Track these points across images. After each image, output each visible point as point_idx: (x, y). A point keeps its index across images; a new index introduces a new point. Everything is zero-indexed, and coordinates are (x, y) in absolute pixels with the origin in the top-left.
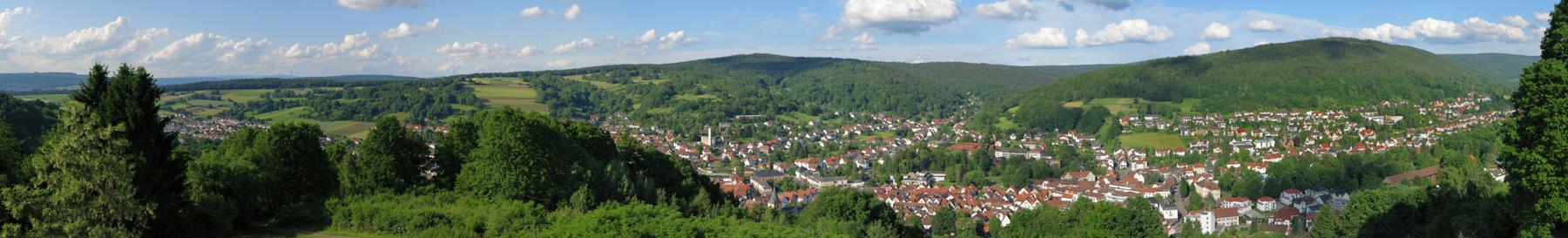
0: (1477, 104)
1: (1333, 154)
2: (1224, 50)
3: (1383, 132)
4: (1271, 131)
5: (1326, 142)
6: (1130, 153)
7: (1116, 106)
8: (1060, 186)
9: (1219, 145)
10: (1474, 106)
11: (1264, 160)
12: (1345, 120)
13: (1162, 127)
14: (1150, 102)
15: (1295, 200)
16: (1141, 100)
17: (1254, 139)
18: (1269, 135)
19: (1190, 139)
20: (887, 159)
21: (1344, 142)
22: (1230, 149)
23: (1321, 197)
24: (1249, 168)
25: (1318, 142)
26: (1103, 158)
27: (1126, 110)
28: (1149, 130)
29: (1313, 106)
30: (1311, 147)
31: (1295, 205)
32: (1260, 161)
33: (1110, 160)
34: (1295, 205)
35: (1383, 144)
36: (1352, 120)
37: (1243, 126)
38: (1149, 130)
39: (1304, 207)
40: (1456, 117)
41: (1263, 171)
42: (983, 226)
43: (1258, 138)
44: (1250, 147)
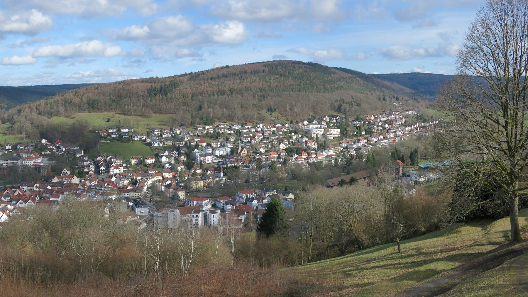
8: (49, 187)
21: (289, 151)
26: (85, 164)
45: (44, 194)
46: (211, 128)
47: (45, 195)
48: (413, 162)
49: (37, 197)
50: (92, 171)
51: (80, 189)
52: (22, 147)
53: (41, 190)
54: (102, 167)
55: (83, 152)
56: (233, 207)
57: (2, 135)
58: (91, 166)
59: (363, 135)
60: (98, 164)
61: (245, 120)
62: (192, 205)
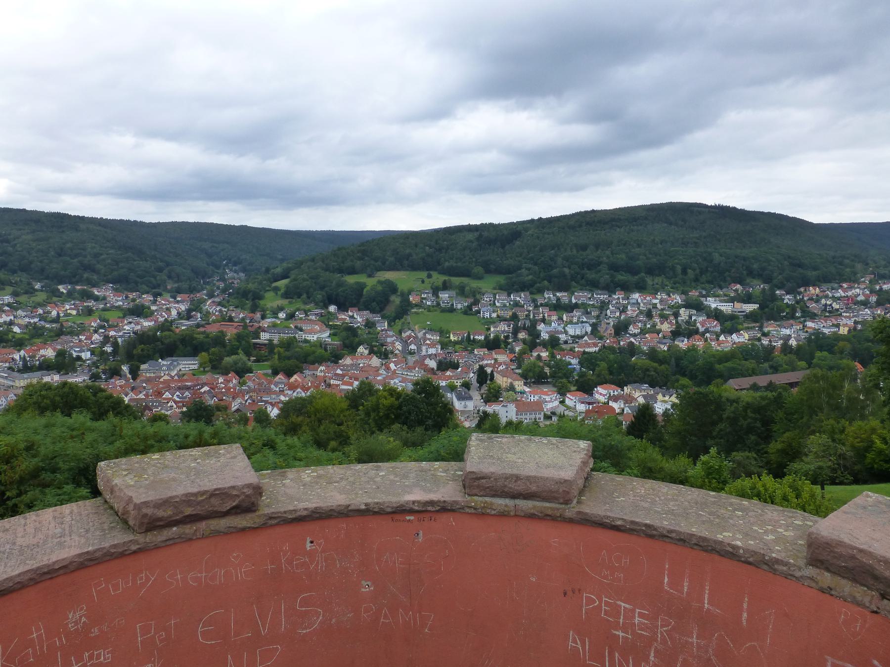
0: (872, 291)
1: (662, 346)
2: (536, 218)
3: (730, 323)
4: (587, 313)
5: (655, 330)
6: (420, 335)
7: (401, 278)
8: (339, 372)
9: (524, 328)
10: (867, 296)
11: (577, 349)
12: (680, 307)
13: (459, 306)
14: (446, 278)
15: (611, 398)
16: (435, 275)
17: (567, 323)
18: (585, 320)
19: (490, 322)
20: (115, 345)
21: (676, 334)
22: (538, 335)
23: (643, 396)
24: (558, 357)
25: (643, 332)
26: (389, 340)
27: (417, 285)
28: (444, 311)
29: (641, 288)
30: (634, 335)
31: (611, 403)
32: (572, 350)
33: (397, 343)
34: (611, 403)
35: (729, 339)
36: (688, 306)
37: (558, 307)
38: (444, 311)
39: (622, 406)
40: (837, 310)
41: (574, 361)
42: (204, 432)
43: (571, 322)
44: (561, 333)
45: (332, 381)
46: (565, 296)
47: (332, 382)
48: (203, 278)
49: (322, 384)
50: (399, 351)
51: (382, 374)
52: (301, 316)
53: (327, 374)
54: (413, 345)
55: (386, 324)
56: (589, 407)
57: (519, 377)
58: (397, 343)
59: (799, 318)
60: (406, 341)
61: (610, 289)
62: (532, 400)
